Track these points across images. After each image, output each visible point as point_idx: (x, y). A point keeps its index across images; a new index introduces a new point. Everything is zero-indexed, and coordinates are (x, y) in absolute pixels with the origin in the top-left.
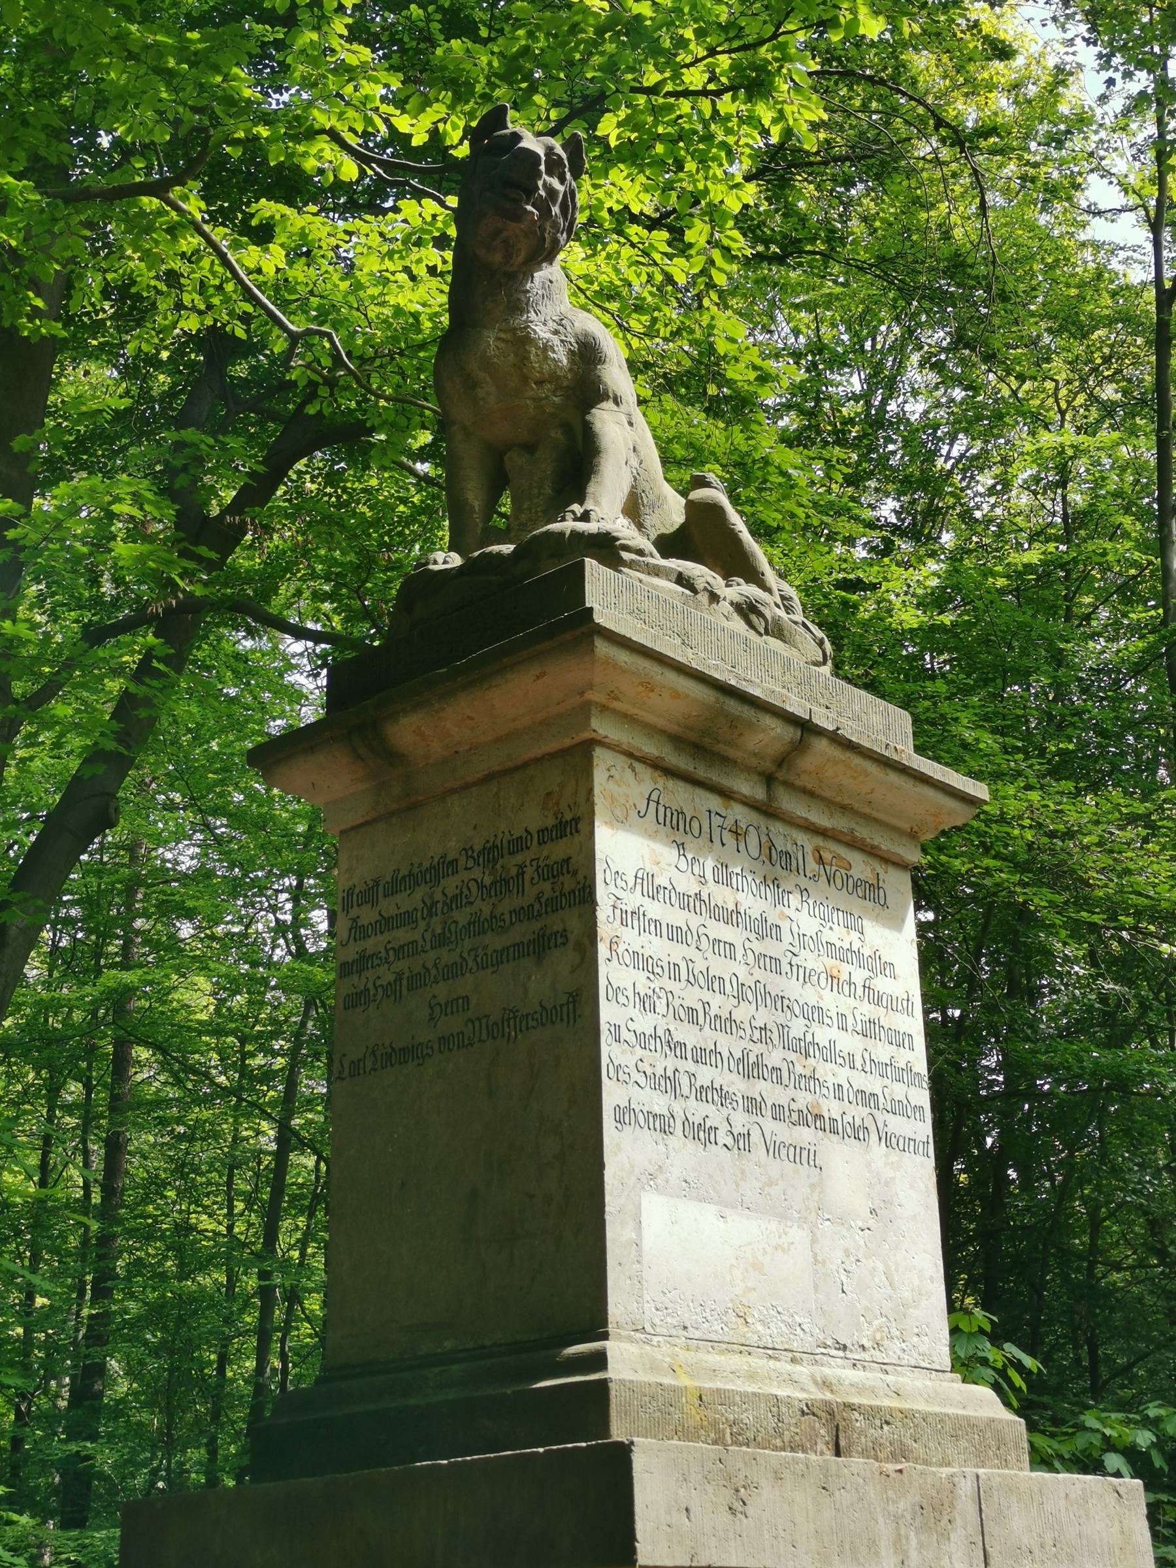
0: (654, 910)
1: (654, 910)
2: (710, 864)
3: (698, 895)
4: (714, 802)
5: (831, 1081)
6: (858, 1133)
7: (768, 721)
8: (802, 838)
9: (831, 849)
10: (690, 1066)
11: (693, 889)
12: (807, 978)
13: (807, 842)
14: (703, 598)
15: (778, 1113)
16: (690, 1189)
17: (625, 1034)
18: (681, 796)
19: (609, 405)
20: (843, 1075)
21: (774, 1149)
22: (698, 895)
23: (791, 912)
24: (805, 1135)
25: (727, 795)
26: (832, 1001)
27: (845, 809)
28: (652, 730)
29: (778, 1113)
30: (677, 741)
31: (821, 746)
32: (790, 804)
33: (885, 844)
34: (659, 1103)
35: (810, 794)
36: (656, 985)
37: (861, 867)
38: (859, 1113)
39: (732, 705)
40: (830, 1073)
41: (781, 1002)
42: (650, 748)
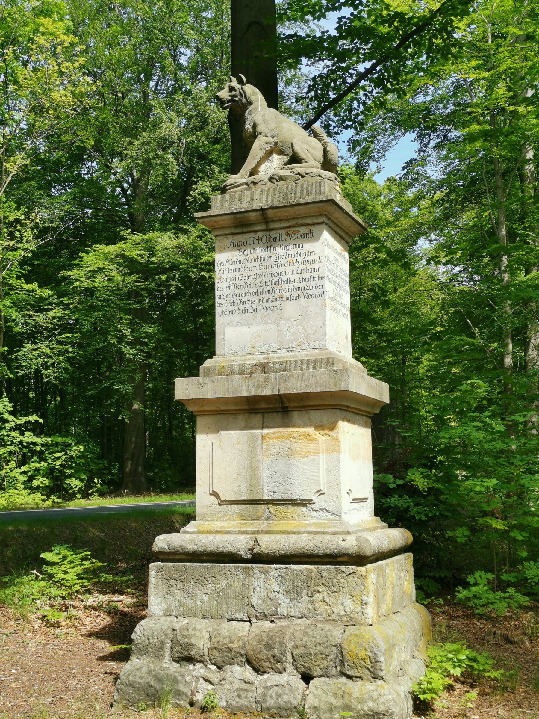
0: (231, 267)
1: (231, 267)
2: (249, 250)
3: (246, 259)
4: (252, 235)
5: (287, 288)
6: (297, 298)
7: (250, 214)
8: (280, 232)
9: (290, 231)
10: (241, 298)
11: (243, 257)
12: (281, 265)
13: (283, 232)
14: (252, 185)
15: (268, 300)
16: (239, 324)
17: (222, 296)
18: (241, 238)
19: (259, 136)
20: (291, 286)
21: (266, 309)
22: (246, 259)
23: (276, 252)
24: (277, 303)
25: (255, 232)
26: (289, 269)
27: (293, 219)
28: (228, 227)
29: (268, 300)
30: (236, 227)
31: (270, 211)
32: (272, 226)
33: (310, 221)
34: (231, 308)
35: (274, 221)
36: (232, 283)
37: (303, 230)
38: (296, 293)
39: (238, 215)
40: (286, 287)
41: (273, 274)
42: (234, 231)
